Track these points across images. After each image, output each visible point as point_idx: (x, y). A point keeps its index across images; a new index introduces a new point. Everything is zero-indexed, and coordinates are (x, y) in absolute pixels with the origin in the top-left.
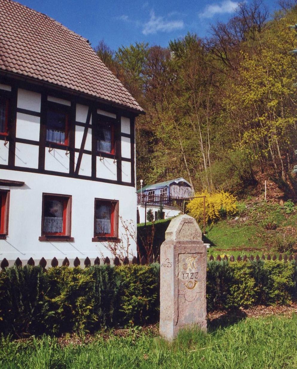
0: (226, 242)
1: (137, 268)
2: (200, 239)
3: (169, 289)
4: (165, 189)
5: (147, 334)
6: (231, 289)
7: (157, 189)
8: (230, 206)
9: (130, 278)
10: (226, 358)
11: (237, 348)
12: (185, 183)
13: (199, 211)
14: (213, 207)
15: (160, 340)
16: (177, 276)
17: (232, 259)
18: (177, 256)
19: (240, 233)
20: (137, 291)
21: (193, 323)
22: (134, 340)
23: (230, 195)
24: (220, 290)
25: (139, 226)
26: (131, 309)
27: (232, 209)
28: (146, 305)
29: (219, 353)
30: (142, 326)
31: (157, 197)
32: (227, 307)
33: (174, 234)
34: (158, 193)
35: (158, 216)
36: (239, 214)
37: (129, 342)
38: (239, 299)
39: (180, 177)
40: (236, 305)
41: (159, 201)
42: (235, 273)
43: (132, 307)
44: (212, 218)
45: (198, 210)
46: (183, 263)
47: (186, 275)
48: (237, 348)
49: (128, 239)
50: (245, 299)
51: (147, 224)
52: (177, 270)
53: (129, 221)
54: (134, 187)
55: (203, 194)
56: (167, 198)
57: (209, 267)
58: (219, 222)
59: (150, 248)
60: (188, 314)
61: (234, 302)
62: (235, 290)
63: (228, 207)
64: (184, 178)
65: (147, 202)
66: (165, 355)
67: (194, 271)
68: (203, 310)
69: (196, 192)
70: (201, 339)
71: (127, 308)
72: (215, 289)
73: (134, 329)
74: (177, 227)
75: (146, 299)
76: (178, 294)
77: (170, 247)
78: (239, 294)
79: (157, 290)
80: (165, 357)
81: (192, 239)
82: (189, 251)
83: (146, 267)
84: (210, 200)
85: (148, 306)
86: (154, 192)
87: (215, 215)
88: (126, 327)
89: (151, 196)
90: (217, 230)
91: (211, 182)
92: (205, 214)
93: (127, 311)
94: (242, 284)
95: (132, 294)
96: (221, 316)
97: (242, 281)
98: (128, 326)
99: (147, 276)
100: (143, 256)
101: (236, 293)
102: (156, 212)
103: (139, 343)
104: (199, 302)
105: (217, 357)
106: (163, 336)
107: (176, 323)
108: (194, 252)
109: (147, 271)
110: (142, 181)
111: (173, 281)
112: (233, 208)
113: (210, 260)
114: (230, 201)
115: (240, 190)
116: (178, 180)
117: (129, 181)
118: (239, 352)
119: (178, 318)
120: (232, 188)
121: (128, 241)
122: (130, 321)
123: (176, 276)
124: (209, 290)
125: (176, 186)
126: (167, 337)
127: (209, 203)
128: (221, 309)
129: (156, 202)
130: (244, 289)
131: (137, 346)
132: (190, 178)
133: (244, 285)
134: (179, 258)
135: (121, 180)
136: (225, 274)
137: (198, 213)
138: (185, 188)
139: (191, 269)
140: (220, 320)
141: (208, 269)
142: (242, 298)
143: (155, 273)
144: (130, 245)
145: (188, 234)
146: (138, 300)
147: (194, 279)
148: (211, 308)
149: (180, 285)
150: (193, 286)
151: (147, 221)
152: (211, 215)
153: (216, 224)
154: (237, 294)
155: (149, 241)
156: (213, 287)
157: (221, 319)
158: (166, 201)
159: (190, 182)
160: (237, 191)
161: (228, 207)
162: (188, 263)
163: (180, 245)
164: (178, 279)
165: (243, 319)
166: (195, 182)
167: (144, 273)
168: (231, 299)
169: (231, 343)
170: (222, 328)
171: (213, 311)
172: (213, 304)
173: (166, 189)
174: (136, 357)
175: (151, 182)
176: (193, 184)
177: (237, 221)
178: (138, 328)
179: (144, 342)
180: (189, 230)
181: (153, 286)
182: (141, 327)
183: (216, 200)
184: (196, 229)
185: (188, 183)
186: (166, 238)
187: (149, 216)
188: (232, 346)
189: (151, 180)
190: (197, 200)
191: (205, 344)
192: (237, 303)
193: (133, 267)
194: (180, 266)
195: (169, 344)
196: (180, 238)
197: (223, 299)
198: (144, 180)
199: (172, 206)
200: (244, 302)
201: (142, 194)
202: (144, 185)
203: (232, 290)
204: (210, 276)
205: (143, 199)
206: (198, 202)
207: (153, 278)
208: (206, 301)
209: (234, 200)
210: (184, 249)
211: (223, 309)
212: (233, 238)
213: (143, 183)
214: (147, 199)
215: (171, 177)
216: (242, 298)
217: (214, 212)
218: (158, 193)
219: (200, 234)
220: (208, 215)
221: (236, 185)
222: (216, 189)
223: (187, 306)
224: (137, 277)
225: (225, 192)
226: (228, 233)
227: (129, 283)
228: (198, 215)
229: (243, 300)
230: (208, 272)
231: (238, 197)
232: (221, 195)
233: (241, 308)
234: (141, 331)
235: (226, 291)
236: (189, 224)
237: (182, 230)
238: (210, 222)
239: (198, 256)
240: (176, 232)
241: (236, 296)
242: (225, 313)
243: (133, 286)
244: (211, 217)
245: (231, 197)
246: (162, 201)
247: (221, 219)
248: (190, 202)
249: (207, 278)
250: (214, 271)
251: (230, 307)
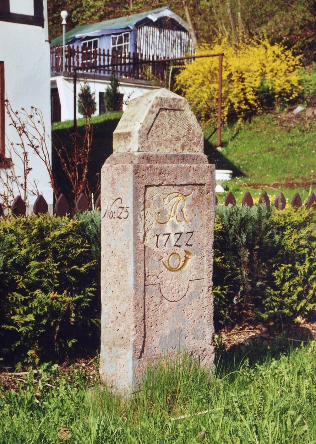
0: (271, 166)
1: (45, 225)
2: (199, 151)
3: (122, 272)
4: (122, 35)
5: (71, 383)
6: (275, 274)
7: (103, 36)
8: (283, 79)
9: (28, 249)
10: (257, 433)
11: (284, 411)
12: (172, 20)
13: (208, 90)
14: (243, 82)
15: (103, 394)
16: (142, 239)
17: (280, 204)
18: (141, 190)
19: (306, 145)
20: (46, 280)
21: (180, 353)
22: (38, 398)
23: (283, 52)
24: (249, 276)
25: (60, 127)
26: (31, 322)
27: (288, 87)
28: (69, 311)
29: (241, 421)
30: (60, 364)
31: (104, 55)
32: (265, 316)
33: (136, 136)
34: (106, 45)
35: (106, 104)
36: (304, 99)
37: (26, 403)
38: (295, 297)
39: (161, 6)
40: (287, 311)
41: (108, 66)
42: (287, 237)
43: (33, 319)
44: (239, 108)
45: (204, 88)
46: (157, 210)
47: (163, 238)
48: (284, 411)
49: (26, 154)
50: (309, 297)
51: (79, 124)
52: (141, 225)
53: (29, 112)
54: (43, 27)
55: (217, 49)
56: (129, 57)
57: (222, 221)
58: (257, 119)
59: (81, 178)
60: (167, 332)
61: (281, 306)
62: (284, 276)
63: (277, 82)
64: (172, 10)
65: (79, 68)
66: (111, 428)
67: (182, 228)
68: (205, 321)
69: (199, 42)
70: (200, 391)
71: (22, 320)
72: (237, 275)
73: (41, 371)
74: (142, 121)
75: (68, 299)
76: (144, 284)
77: (124, 169)
78: (295, 286)
79: (95, 274)
80: (112, 433)
81: (179, 150)
82: (170, 179)
83: (66, 223)
84: (235, 63)
85: (73, 315)
86: (96, 42)
87: (246, 100)
88: (19, 366)
89: (90, 53)
90: (250, 139)
91: (240, 19)
92: (222, 99)
93: (21, 329)
94: (302, 264)
95: (33, 286)
96: (251, 338)
97: (303, 256)
98: (25, 364)
99: (71, 243)
100: (61, 195)
101: (287, 284)
102: (101, 94)
103: (50, 404)
104: (195, 303)
105: (236, 431)
106: (109, 385)
107: (140, 354)
108: (184, 183)
109: (72, 231)
110: (64, 14)
111: (132, 252)
112: (292, 85)
113: (226, 204)
114: (284, 66)
115: (310, 40)
116: (155, 13)
117: (30, 11)
118: (289, 419)
119: (144, 342)
120: (289, 35)
121: (26, 161)
122: (30, 352)
123: (139, 241)
124: (219, 276)
125: (151, 29)
126: (118, 387)
127: (233, 70)
128: (250, 323)
129: (99, 68)
130: (307, 275)
131: (44, 411)
132: (186, 9)
133: (308, 265)
134: (148, 195)
135: (9, 11)
136: (261, 239)
137: (205, 95)
138: (172, 35)
139: (177, 223)
140: (248, 348)
141: (220, 226)
142: (301, 297)
143: (92, 236)
144: (30, 169)
145: (169, 136)
146: (49, 301)
147: (184, 247)
148: (227, 320)
149: (149, 262)
150: (181, 264)
151: (79, 116)
152: (235, 101)
153: (247, 122)
154: (290, 286)
155: (79, 159)
156: (232, 269)
157: (249, 346)
158: (125, 64)
159: (185, 20)
160: (303, 42)
161: (277, 82)
162: (170, 208)
163: (148, 165)
164: (145, 247)
165: (302, 345)
166: (199, 20)
167: (62, 236)
168: (275, 298)
169: (270, 397)
170: (250, 364)
171: (233, 327)
172: (232, 309)
173: (126, 36)
174: (39, 434)
175: (90, 17)
176: (195, 25)
177: (298, 116)
178: (49, 367)
179: (62, 401)
180: (171, 127)
181: (86, 266)
182: (56, 365)
183: (249, 63)
184: (189, 125)
185: (180, 21)
186: (114, 146)
187: (85, 102)
188: (271, 405)
189: (89, 13)
190: (202, 64)
191: (209, 401)
192: (291, 308)
193: (36, 222)
194: (148, 216)
195: (123, 402)
196: (149, 147)
197: (257, 298)
198: (70, 12)
199: (142, 79)
200: (306, 305)
201: (65, 47)
202: (71, 25)
203: (278, 276)
204: (223, 243)
205: (70, 60)
206: (205, 68)
207: (86, 248)
208: (212, 300)
209: (294, 63)
210: (160, 173)
211: (254, 323)
212: (287, 157)
213: (68, 19)
214: (79, 60)
215: (140, 5)
216: (301, 297)
217: (245, 94)
218: (106, 45)
219: (200, 137)
220: (230, 101)
221: (301, 27)
222: (251, 35)
223: (165, 312)
224: (45, 246)
225: (272, 44)
226: (278, 146)
227: (27, 260)
228: (204, 102)
229: (304, 301)
230: (217, 233)
231: (305, 56)
232: (263, 50)
233: (299, 319)
234: (56, 374)
235: (263, 279)
236: (172, 113)
237: (154, 128)
238: (232, 117)
239: (195, 192)
240: (139, 132)
241: (287, 291)
242: (261, 330)
243: (36, 267)
244: (236, 105)
245: (287, 56)
246: (117, 65)
247: (259, 110)
248: (184, 69)
249: (215, 246)
250: (235, 231)
251: (273, 317)
